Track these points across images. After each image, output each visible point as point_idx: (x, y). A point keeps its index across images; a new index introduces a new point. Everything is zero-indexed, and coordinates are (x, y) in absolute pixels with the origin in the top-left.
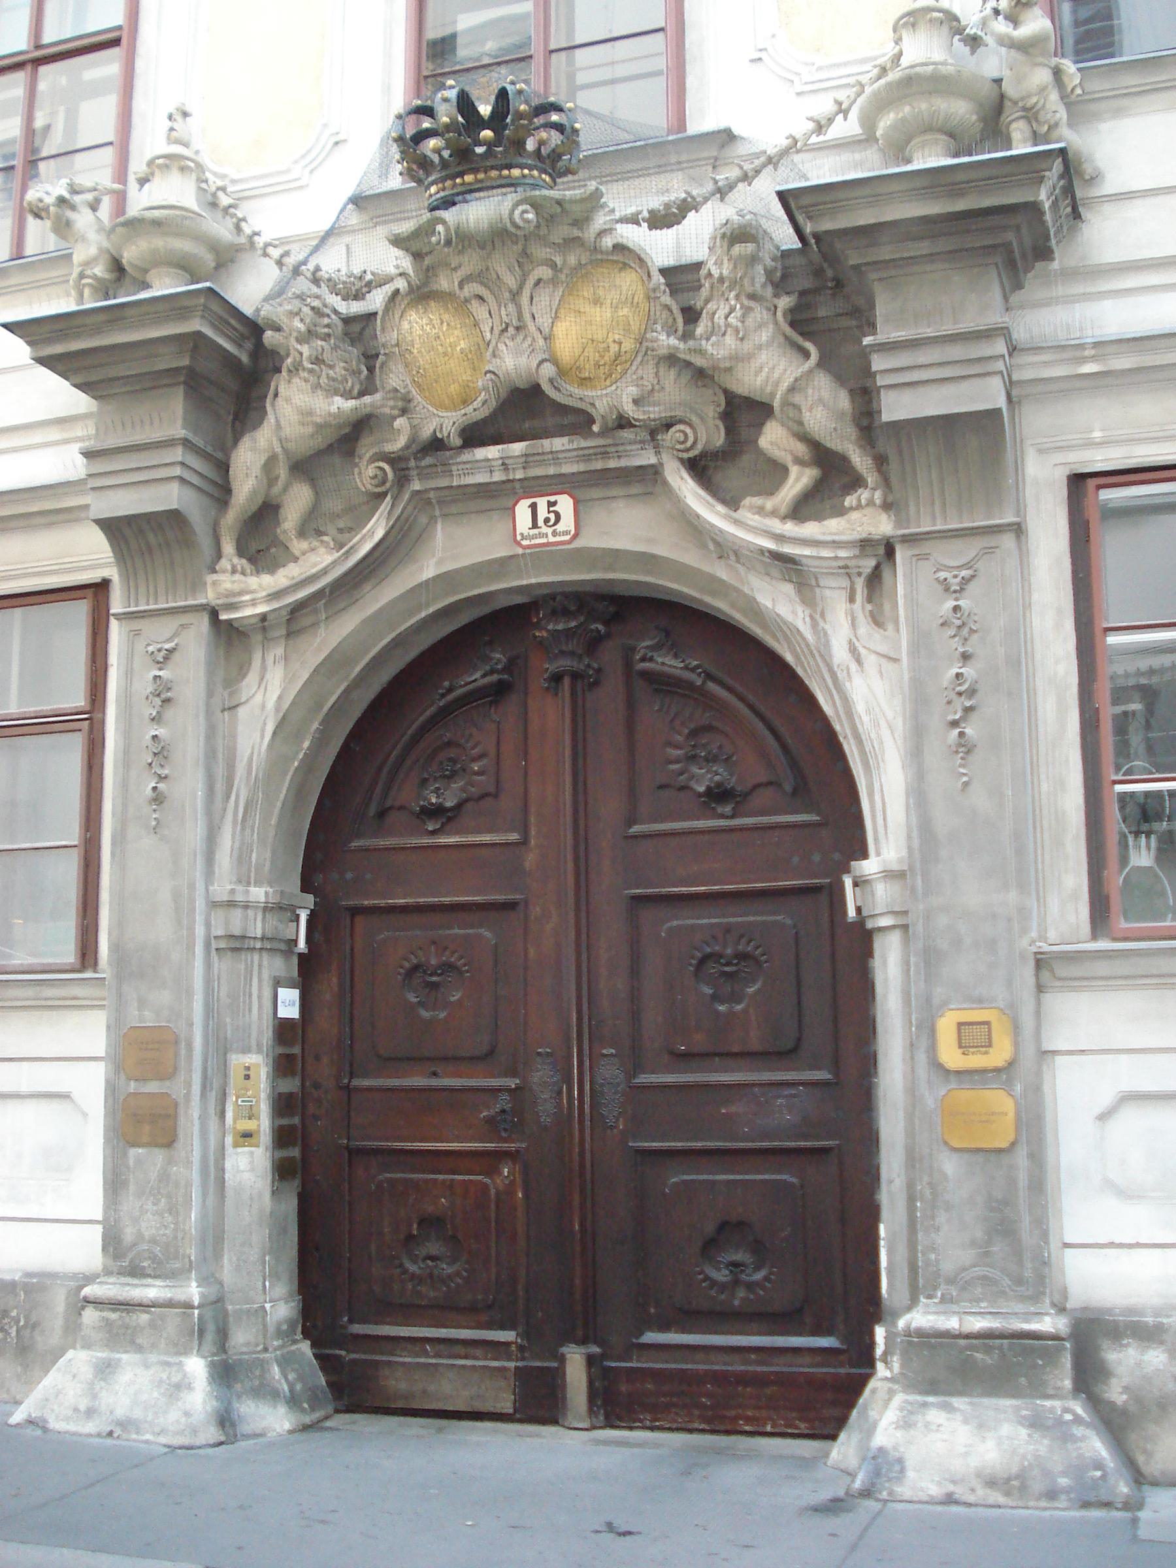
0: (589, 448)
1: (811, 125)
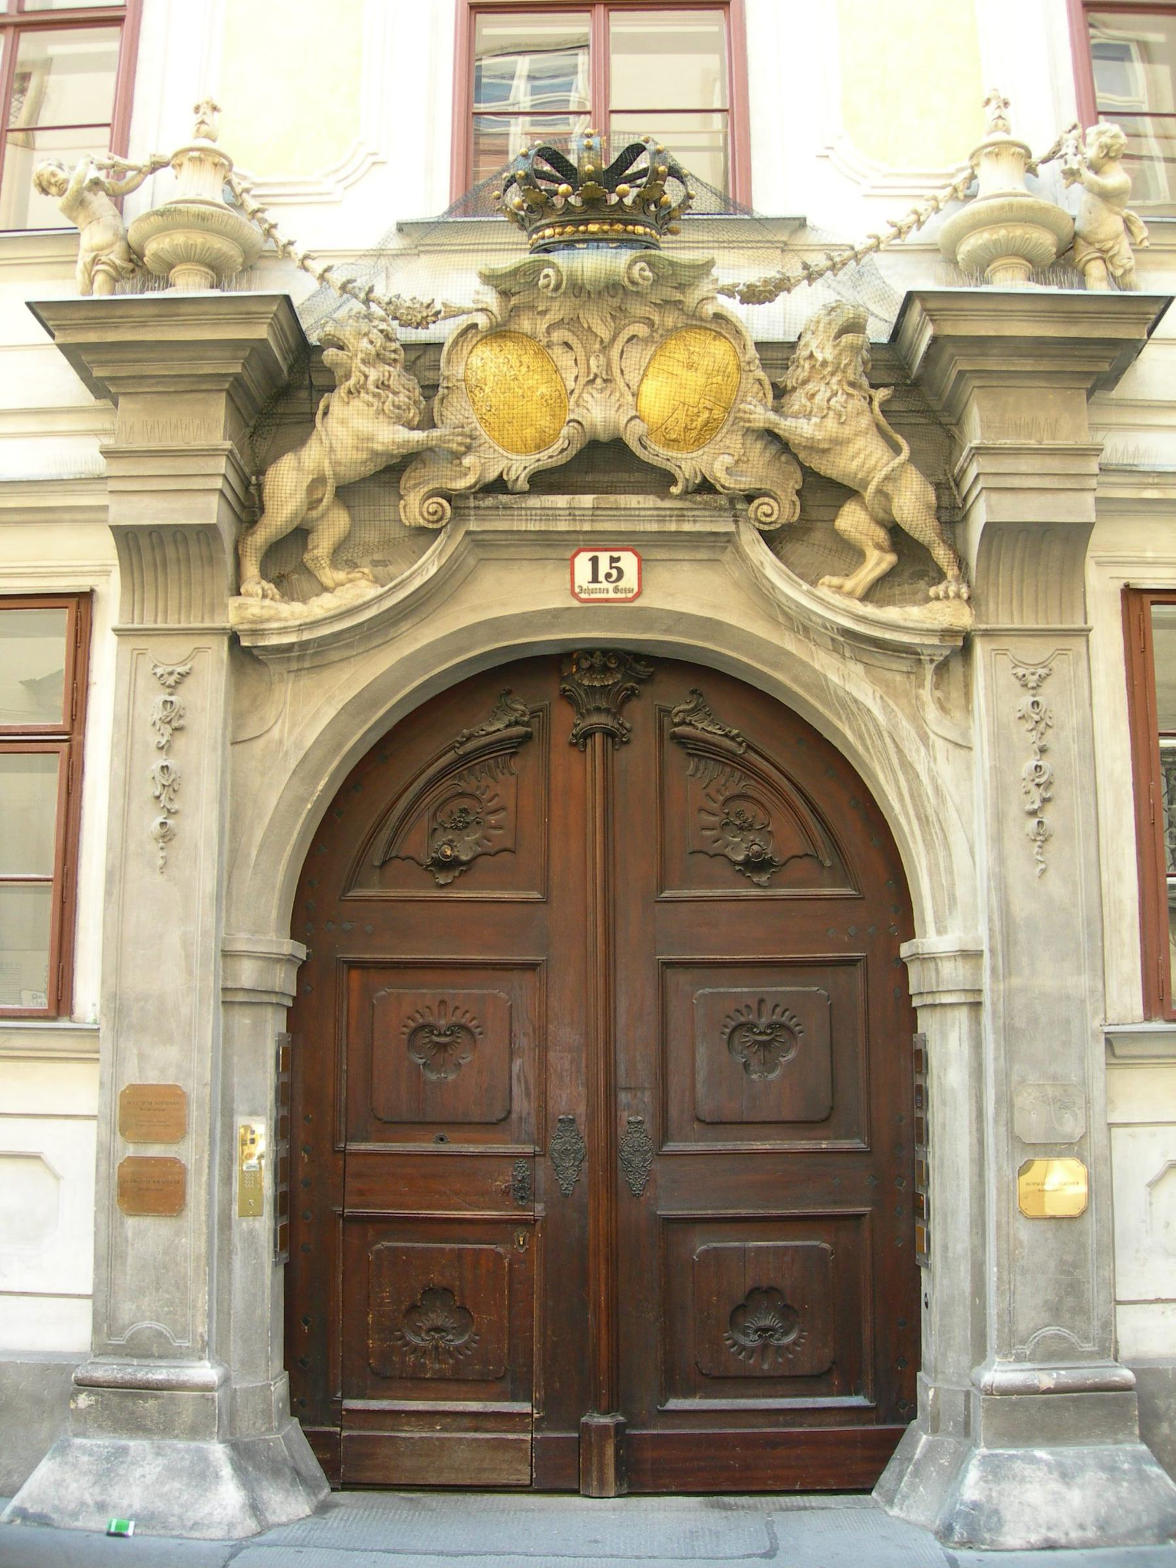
0: (665, 509)
1: (894, 230)
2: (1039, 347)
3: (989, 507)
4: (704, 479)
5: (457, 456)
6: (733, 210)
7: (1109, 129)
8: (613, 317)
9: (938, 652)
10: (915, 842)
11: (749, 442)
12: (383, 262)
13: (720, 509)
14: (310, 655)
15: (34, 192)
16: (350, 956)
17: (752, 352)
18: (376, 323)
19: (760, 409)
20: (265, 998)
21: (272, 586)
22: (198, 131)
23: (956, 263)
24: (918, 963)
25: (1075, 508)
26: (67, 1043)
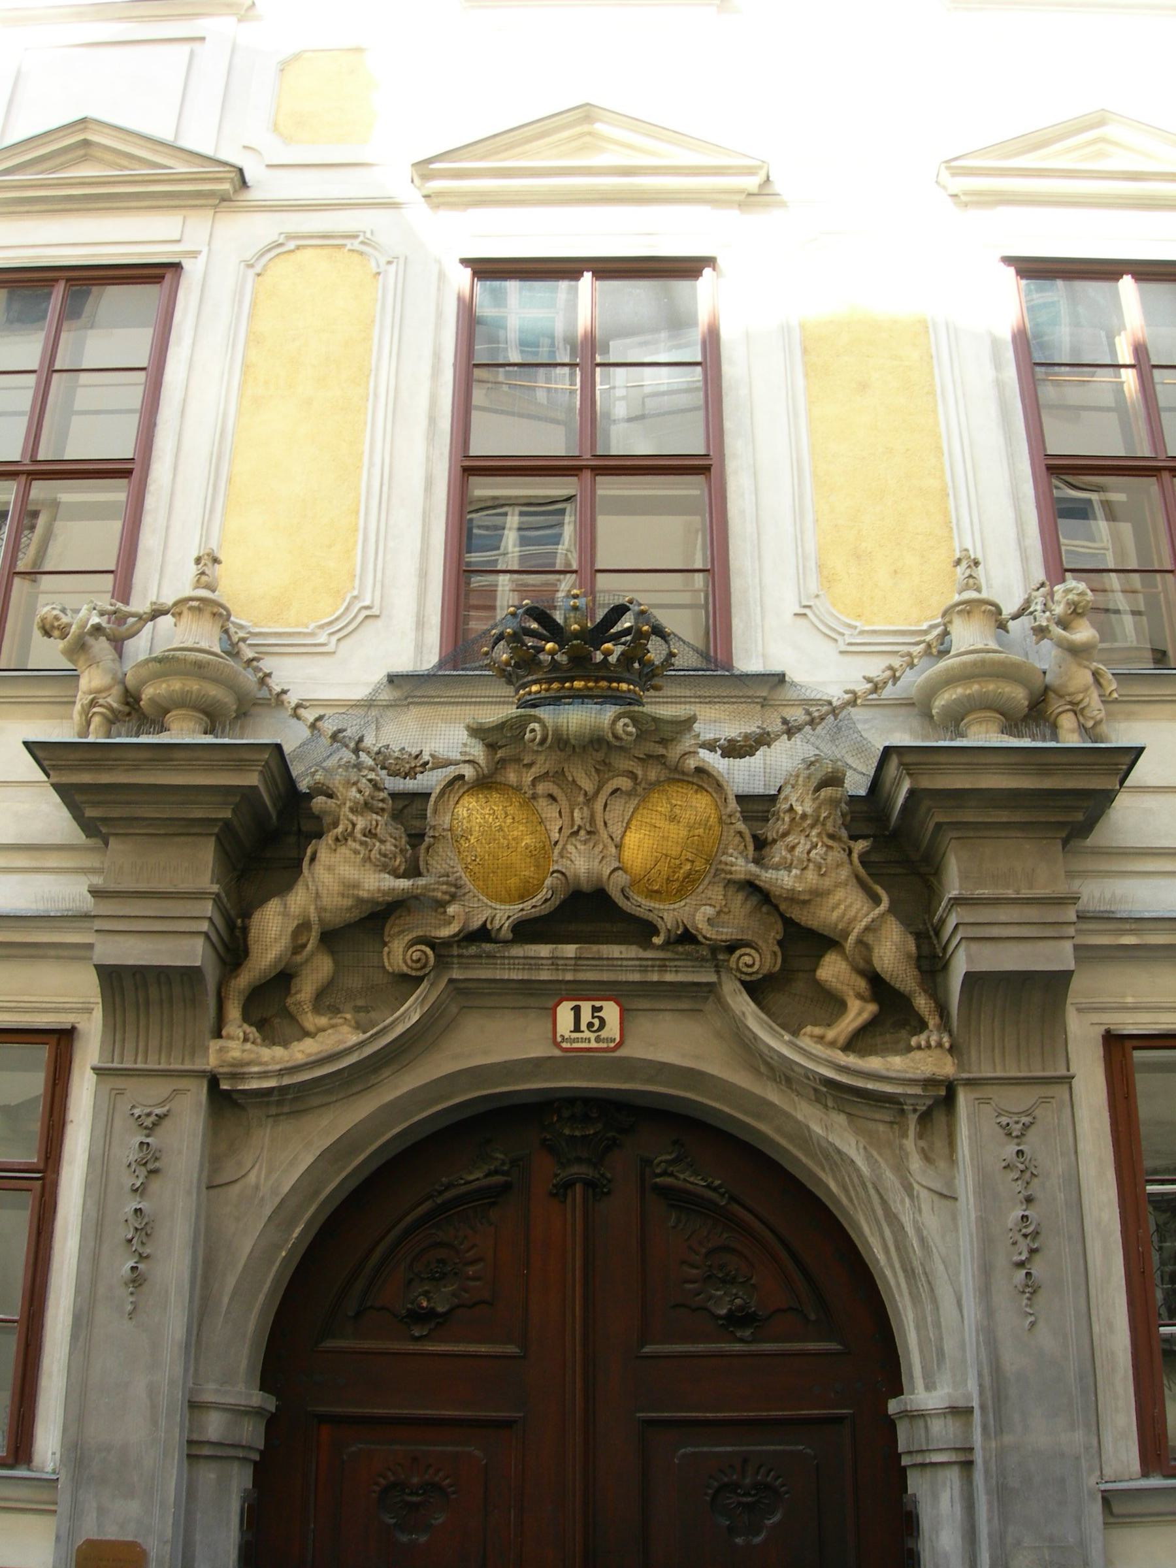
0: (647, 959)
2: (1013, 798)
3: (970, 958)
4: (686, 930)
5: (441, 905)
6: (716, 671)
7: (1076, 585)
8: (597, 770)
9: (921, 1102)
10: (901, 1295)
11: (730, 893)
12: (374, 712)
13: (704, 959)
14: (291, 1099)
15: (37, 634)
16: (322, 1409)
17: (733, 805)
18: (365, 772)
19: (741, 861)
20: (232, 1452)
21: (254, 1029)
22: (198, 581)
23: (932, 717)
24: (906, 1420)
25: (1056, 956)
26: (23, 1492)
